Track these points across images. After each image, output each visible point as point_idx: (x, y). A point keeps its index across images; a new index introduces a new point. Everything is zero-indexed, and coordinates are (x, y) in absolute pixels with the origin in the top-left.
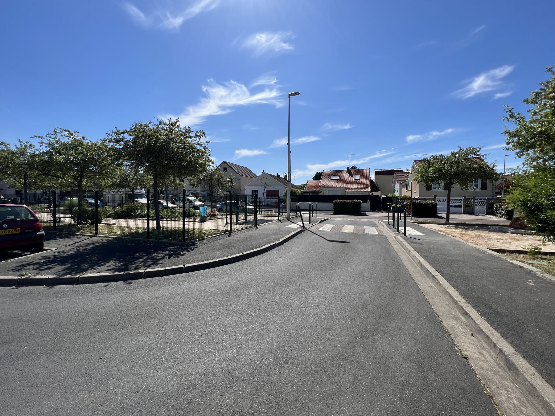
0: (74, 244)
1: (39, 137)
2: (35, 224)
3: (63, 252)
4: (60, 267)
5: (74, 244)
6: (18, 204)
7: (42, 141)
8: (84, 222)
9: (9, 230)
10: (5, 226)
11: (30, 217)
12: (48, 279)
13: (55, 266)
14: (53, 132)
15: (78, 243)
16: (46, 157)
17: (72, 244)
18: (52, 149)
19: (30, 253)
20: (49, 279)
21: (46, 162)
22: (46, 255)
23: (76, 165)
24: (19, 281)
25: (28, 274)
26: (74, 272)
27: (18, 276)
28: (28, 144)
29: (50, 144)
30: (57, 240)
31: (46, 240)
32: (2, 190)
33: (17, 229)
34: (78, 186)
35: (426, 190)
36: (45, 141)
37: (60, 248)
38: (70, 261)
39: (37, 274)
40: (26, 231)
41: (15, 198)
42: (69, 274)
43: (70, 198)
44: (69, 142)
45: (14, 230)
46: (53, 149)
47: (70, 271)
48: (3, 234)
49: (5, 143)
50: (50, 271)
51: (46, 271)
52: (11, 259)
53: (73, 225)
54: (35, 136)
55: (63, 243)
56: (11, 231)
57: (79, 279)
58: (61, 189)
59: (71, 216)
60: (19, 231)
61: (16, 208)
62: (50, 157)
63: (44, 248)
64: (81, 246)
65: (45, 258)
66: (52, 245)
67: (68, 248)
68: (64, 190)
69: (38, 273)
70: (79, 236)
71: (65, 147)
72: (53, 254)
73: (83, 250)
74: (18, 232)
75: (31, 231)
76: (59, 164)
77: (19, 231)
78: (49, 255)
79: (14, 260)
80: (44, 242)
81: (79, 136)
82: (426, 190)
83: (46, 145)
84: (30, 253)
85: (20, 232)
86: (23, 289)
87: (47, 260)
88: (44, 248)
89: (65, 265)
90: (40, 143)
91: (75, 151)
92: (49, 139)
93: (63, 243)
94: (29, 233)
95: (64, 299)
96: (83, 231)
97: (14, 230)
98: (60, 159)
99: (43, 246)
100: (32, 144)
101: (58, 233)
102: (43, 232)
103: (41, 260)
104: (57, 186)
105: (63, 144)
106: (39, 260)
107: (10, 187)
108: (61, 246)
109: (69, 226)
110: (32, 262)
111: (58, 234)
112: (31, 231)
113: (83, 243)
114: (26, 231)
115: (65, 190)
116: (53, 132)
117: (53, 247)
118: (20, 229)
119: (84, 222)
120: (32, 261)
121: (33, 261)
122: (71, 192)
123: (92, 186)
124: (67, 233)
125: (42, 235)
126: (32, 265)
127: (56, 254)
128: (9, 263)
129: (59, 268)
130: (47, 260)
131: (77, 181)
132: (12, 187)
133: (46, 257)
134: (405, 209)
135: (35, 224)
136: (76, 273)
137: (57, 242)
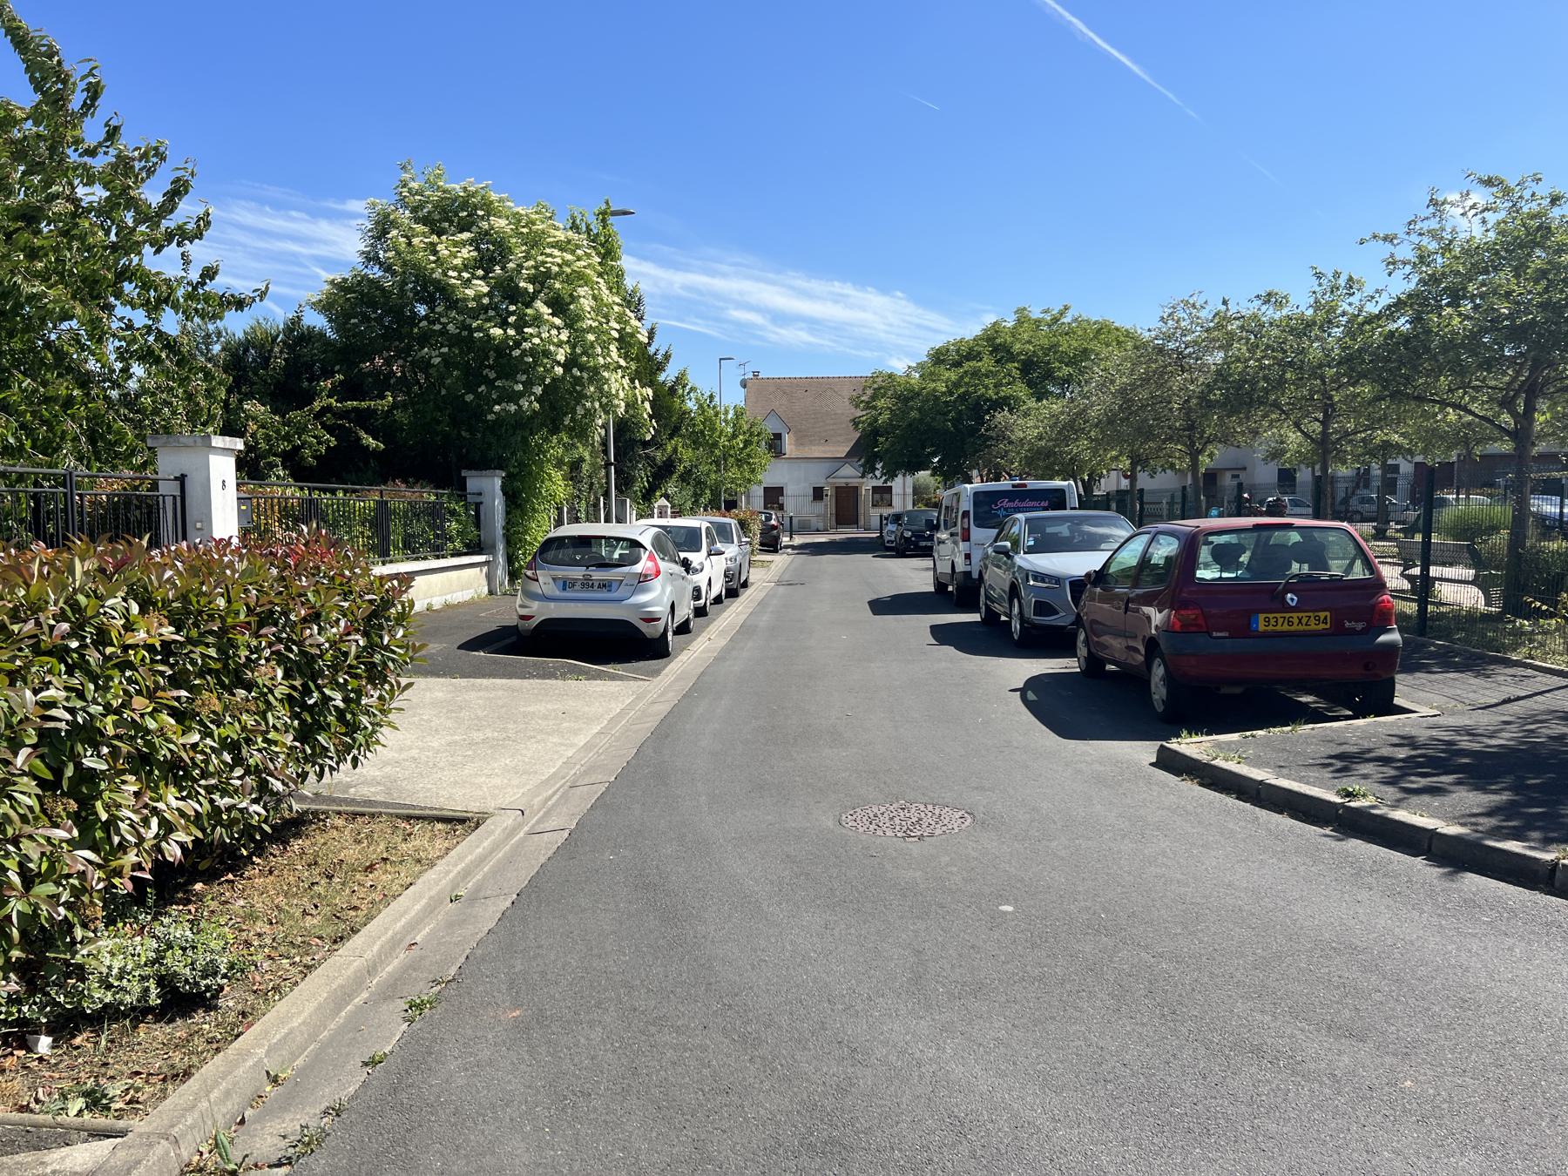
0: (1505, 702)
1: (1385, 239)
2: (1373, 601)
3: (1470, 732)
4: (1471, 795)
5: (1505, 702)
6: (1325, 519)
7: (1392, 255)
8: (1544, 608)
9: (1300, 615)
10: (1292, 600)
11: (1358, 572)
12: (1433, 834)
13: (1452, 788)
14: (1428, 206)
15: (1521, 703)
16: (1402, 324)
17: (1495, 701)
18: (1425, 284)
19: (1350, 713)
20: (1438, 833)
21: (1406, 339)
22: (1407, 731)
23: (1517, 334)
24: (1340, 812)
25: (1370, 797)
26: (1535, 835)
27: (1338, 793)
28: (1342, 282)
29: (1423, 258)
30: (1437, 676)
31: (1410, 669)
32: (1245, 469)
33: (1322, 615)
34: (1513, 435)
35: (931, 627)
36: (1405, 252)
37: (1453, 713)
38: (1508, 780)
39: (1396, 805)
40: (1347, 624)
41: (1278, 499)
42: (1517, 835)
43: (1458, 494)
44: (1490, 234)
45: (1312, 618)
46: (1434, 279)
47: (1515, 820)
48: (1286, 627)
49: (1276, 294)
50: (1436, 802)
51: (1426, 798)
52: (1208, 734)
53: (1486, 617)
54: (1375, 237)
55: (1459, 692)
56: (1304, 621)
57: (1558, 874)
58: (1426, 458)
59: (1477, 576)
60: (1326, 623)
61: (1316, 534)
62: (1417, 320)
63: (1396, 701)
64: (1533, 718)
65: (1405, 742)
66: (1421, 694)
67: (1485, 720)
68: (1435, 458)
69: (1399, 801)
70: (1520, 671)
71: (1479, 260)
72: (1434, 733)
73: (1550, 738)
74: (1322, 626)
75: (1360, 626)
76: (1450, 345)
77: (1326, 623)
78: (1423, 735)
79: (1313, 729)
80: (1399, 677)
81: (1539, 194)
82: (931, 627)
83: (1408, 268)
84: (1350, 713)
85: (1328, 626)
86: (1357, 847)
87: (1419, 752)
88: (1396, 701)
89: (1486, 791)
90: (1389, 263)
91: (1518, 272)
92: (1415, 238)
93: (1459, 692)
94: (1353, 632)
95: (1509, 941)
96: (1537, 648)
97: (1312, 618)
98: (1454, 320)
99: (1391, 694)
100: (1355, 277)
101: (1434, 645)
102: (1394, 637)
103: (1396, 749)
104: (1411, 441)
105: (1470, 251)
106: (1392, 749)
107: (1268, 456)
108: (1454, 703)
109: (1469, 620)
110: (1370, 751)
111: (1432, 648)
112: (1360, 626)
113: (1542, 708)
114: (1347, 624)
115: (1438, 460)
116: (1428, 206)
117: (1426, 704)
118: (1328, 614)
119: (1544, 608)
120: (1366, 745)
121: (1372, 746)
122: (1456, 466)
123: (1553, 434)
124: (1468, 651)
125: (1391, 646)
126: (1372, 764)
127: (1446, 736)
128: (1301, 735)
129: (1473, 800)
130: (1419, 752)
131: (1514, 414)
132: (1272, 459)
133: (1409, 741)
134: (491, 367)
135: (1373, 601)
136: (1546, 843)
137: (1436, 686)
